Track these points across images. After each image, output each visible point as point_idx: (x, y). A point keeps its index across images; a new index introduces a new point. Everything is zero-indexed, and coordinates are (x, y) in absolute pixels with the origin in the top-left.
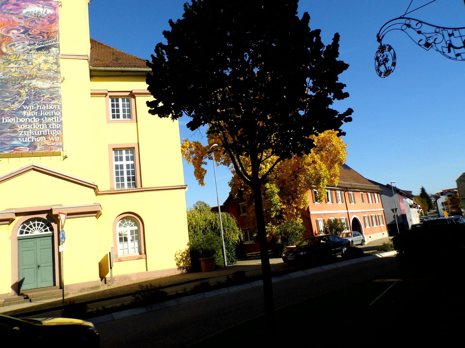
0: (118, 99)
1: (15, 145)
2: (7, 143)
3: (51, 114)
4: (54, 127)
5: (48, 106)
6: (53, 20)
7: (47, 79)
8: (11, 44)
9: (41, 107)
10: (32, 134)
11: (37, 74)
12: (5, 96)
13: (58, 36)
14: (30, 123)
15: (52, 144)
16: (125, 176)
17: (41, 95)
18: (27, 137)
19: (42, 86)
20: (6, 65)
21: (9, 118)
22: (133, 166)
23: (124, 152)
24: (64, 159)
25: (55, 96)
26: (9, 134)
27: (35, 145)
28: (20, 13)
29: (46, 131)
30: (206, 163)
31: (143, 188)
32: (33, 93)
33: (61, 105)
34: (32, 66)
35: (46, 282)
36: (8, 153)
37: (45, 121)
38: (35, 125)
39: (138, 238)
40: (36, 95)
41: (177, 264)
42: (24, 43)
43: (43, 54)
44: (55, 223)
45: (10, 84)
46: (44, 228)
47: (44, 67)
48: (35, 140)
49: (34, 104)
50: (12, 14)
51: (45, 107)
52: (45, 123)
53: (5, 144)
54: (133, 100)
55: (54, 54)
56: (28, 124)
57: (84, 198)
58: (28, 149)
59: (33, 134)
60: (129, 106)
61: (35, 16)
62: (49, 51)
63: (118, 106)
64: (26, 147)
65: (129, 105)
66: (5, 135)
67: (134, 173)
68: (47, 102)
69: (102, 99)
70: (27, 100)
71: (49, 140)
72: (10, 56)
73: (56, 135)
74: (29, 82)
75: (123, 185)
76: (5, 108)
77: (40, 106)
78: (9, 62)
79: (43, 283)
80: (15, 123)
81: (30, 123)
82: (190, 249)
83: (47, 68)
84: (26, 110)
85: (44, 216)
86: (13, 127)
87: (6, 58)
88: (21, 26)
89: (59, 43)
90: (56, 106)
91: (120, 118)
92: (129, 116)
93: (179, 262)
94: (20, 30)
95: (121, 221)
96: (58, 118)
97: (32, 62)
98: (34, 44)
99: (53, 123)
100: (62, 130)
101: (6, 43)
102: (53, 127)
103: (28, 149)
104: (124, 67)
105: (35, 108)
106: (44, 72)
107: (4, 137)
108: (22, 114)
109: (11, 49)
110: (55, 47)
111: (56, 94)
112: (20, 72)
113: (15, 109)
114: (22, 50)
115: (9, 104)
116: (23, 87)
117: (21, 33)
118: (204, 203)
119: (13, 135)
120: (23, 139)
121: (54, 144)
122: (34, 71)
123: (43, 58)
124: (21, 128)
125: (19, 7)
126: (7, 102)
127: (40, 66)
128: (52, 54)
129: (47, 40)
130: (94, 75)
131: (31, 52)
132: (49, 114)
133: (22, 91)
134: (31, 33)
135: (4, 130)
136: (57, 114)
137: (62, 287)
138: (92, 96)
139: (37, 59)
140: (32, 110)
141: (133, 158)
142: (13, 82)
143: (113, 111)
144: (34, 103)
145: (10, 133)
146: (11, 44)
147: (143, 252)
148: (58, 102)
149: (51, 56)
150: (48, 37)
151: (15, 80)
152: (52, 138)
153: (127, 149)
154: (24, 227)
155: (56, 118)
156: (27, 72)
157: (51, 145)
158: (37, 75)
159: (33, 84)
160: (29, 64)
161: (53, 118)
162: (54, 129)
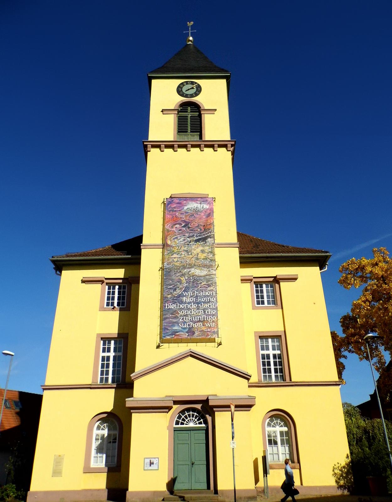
0: (262, 284)
1: (176, 331)
2: (169, 329)
3: (207, 300)
4: (210, 313)
5: (205, 293)
6: (210, 214)
7: (204, 267)
8: (174, 237)
9: (199, 294)
10: (190, 319)
11: (196, 263)
12: (169, 283)
13: (213, 228)
14: (189, 309)
15: (209, 330)
16: (272, 367)
17: (198, 282)
18: (186, 323)
19: (199, 274)
20: (170, 255)
21: (171, 305)
22: (280, 356)
23: (270, 340)
24: (218, 346)
25: (211, 283)
26: (171, 320)
27: (193, 331)
28: (182, 209)
29: (203, 317)
30: (346, 356)
31: (293, 382)
32: (191, 280)
33: (216, 291)
34: (191, 256)
35: (200, 484)
36: (170, 339)
37: (202, 306)
38: (193, 311)
39: (289, 442)
40: (195, 282)
41: (336, 481)
42: (185, 235)
43: (201, 244)
44: (209, 416)
45: (173, 272)
46: (198, 420)
47: (202, 256)
48: (193, 325)
49: (193, 291)
50: (175, 211)
51: (202, 293)
52: (202, 308)
53: (168, 330)
54: (277, 285)
55: (210, 244)
56: (187, 310)
57: (235, 388)
58: (187, 334)
59: (192, 320)
60: (274, 292)
61: (194, 211)
62: (206, 241)
63: (262, 291)
64: (185, 333)
65: (272, 290)
66: (167, 320)
67: (281, 363)
68: (204, 289)
69: (98, 286)
70: (186, 287)
71: (206, 326)
72: (173, 247)
73: (212, 321)
74: (189, 270)
75: (270, 377)
76: (168, 295)
77: (197, 292)
78: (172, 253)
79: (197, 483)
80: (176, 309)
81: (189, 309)
82: (352, 461)
83: (204, 257)
84: (185, 296)
85: (199, 406)
86: (175, 313)
87: (170, 249)
88: (182, 221)
89: (214, 234)
90: (212, 292)
91: (264, 304)
92: (273, 302)
93: (339, 479)
94: (182, 224)
95: (269, 419)
96: (213, 304)
97: (191, 252)
98: (193, 236)
99: (209, 309)
100: (217, 316)
101: (171, 236)
102: (209, 313)
103: (187, 334)
104: (269, 253)
105: (193, 294)
106: (201, 261)
107: (166, 323)
108: (182, 300)
109: (174, 242)
110: (211, 238)
111: (212, 281)
112: (181, 261)
113: (176, 296)
114: (183, 242)
115: (172, 291)
116: (183, 275)
117: (182, 227)
118: (351, 406)
119: (175, 320)
120: (183, 324)
121: (210, 330)
122: (192, 260)
123: (201, 248)
124: (181, 314)
125: (181, 205)
126: (170, 289)
127: (198, 256)
128: (208, 244)
129: (204, 232)
130: (245, 262)
131: (190, 244)
132: (206, 300)
133: (183, 279)
134: (190, 226)
135: (167, 316)
136: (213, 300)
137: (216, 492)
138: (242, 282)
139: (196, 250)
140: (191, 297)
141: (280, 348)
142: (176, 271)
143: (258, 297)
144: (192, 290)
145: (172, 318)
146: (174, 237)
147: (296, 460)
148: (213, 289)
149: (208, 246)
150: (205, 229)
151: (177, 269)
152: (208, 324)
153: (273, 337)
154: (179, 417)
155: (212, 304)
156: (187, 261)
157: (208, 331)
158: (195, 264)
159: (192, 272)
160: (188, 254)
161: (209, 304)
162: (210, 315)
